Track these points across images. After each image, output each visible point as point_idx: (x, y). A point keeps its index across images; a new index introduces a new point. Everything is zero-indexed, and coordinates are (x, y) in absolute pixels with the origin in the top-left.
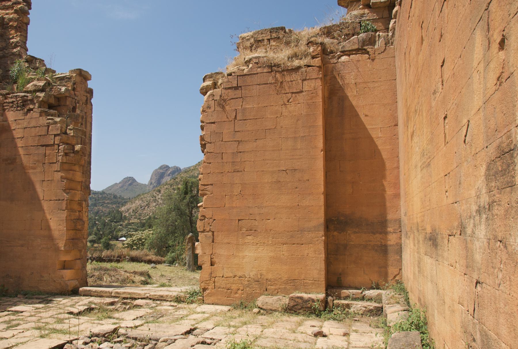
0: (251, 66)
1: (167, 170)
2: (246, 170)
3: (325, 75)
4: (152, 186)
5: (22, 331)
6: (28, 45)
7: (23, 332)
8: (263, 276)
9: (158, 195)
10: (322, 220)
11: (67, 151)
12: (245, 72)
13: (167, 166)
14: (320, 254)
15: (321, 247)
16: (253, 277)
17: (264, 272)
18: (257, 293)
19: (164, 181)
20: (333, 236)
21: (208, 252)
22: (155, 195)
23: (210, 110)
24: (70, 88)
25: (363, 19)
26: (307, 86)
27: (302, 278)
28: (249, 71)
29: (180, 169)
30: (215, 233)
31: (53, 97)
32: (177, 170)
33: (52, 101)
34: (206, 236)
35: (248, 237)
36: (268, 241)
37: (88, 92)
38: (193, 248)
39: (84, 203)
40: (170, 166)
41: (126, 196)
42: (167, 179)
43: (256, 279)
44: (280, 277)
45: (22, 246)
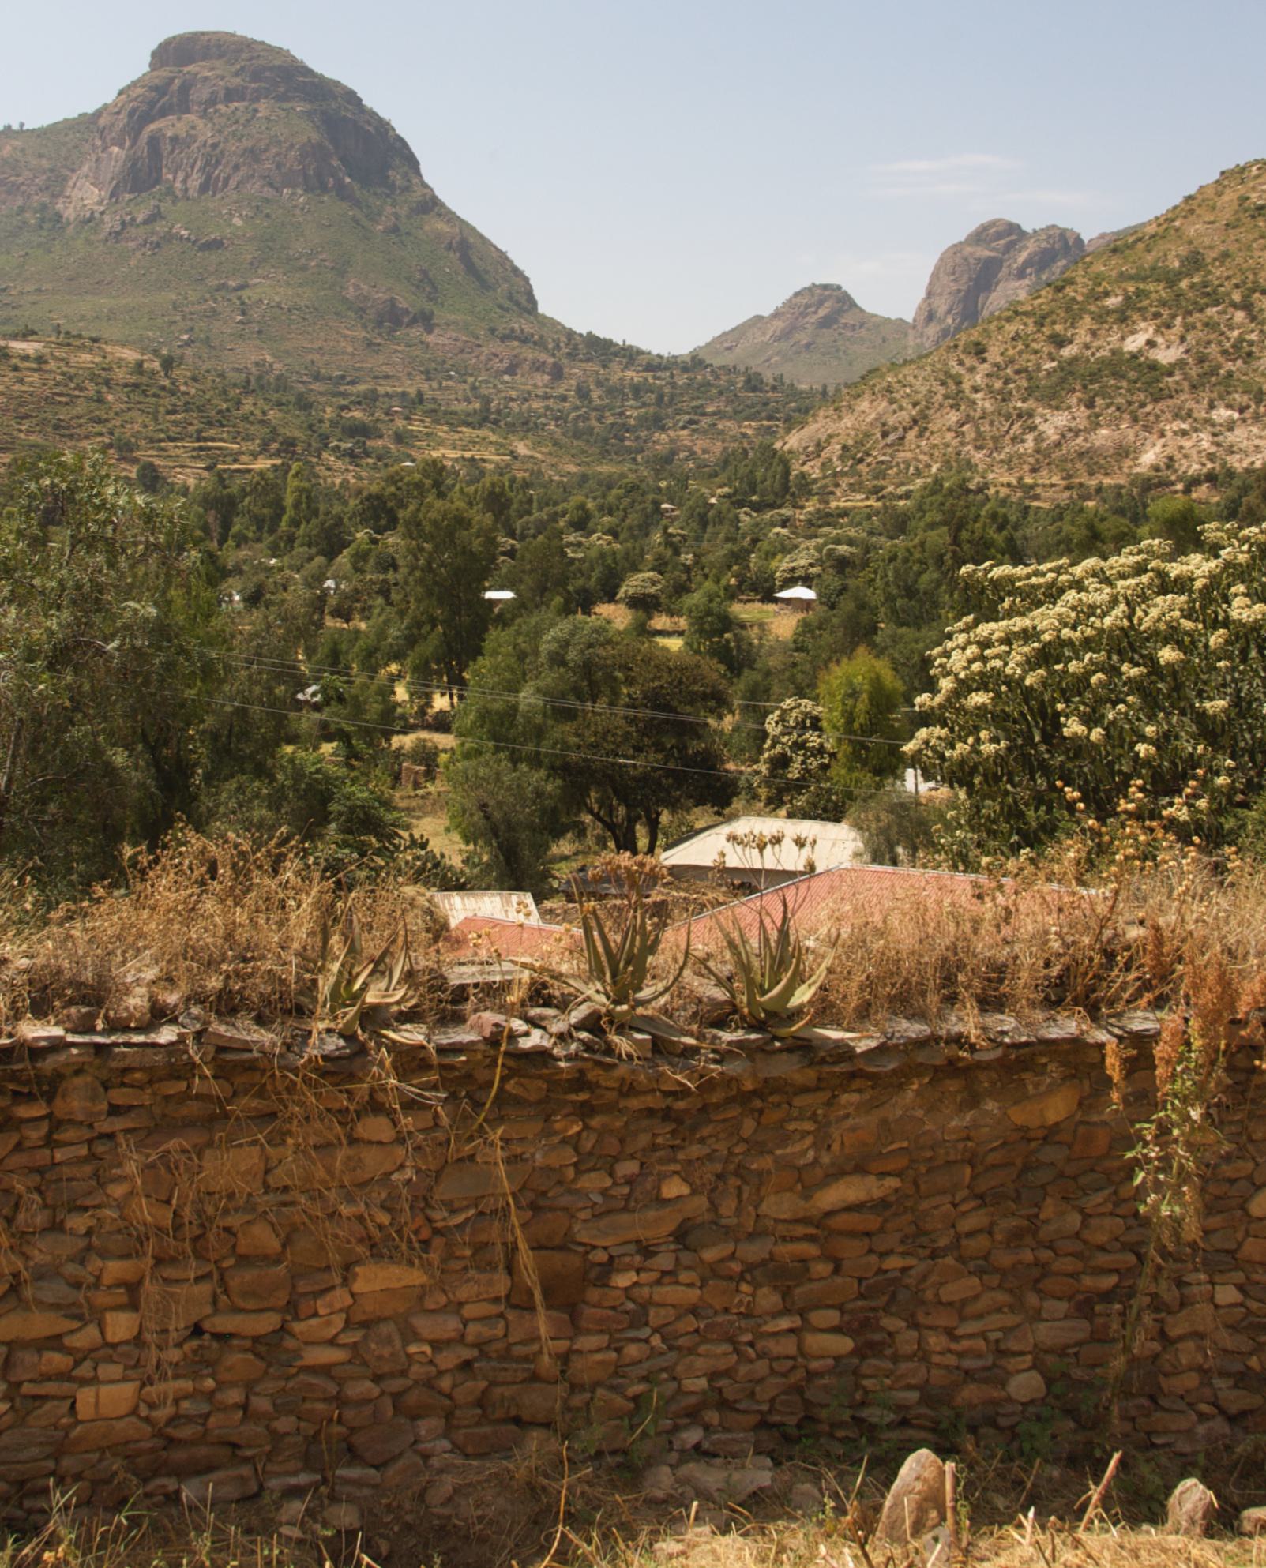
1: (1010, 246)
9: (972, 370)
29: (1078, 240)
32: (1062, 246)
40: (1028, 228)
41: (806, 377)
42: (1011, 291)
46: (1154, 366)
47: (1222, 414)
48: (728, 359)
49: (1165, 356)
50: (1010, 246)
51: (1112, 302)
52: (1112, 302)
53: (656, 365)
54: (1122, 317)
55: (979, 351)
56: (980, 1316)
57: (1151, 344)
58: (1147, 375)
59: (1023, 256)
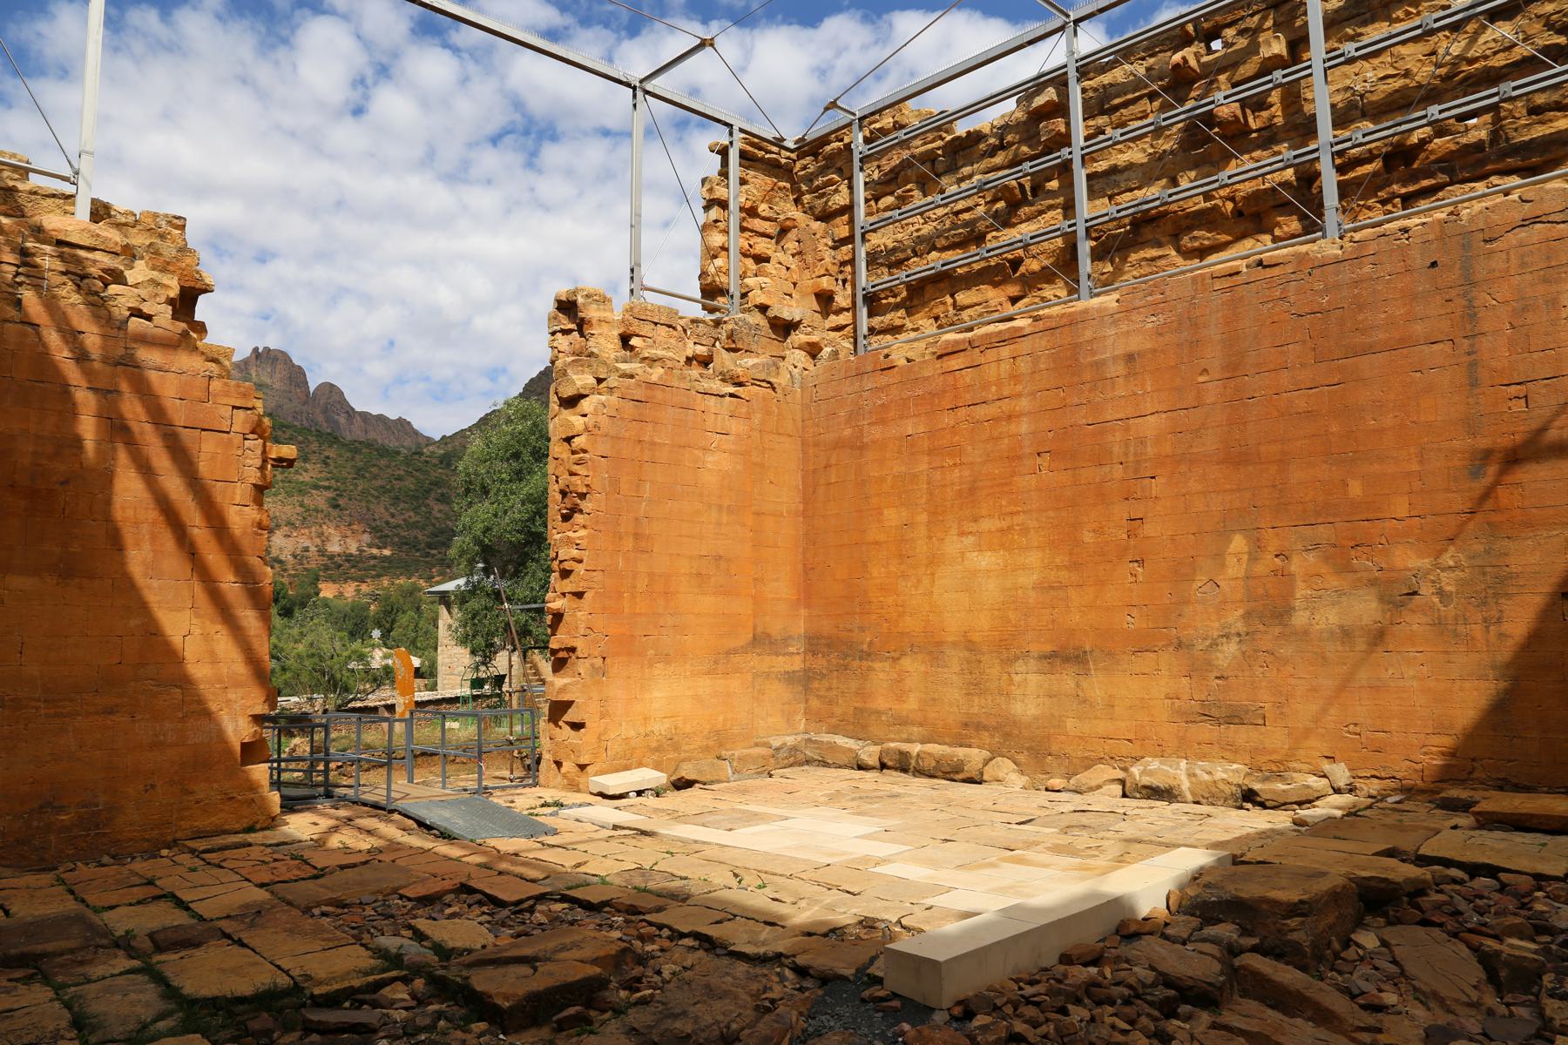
45: (110, 711)
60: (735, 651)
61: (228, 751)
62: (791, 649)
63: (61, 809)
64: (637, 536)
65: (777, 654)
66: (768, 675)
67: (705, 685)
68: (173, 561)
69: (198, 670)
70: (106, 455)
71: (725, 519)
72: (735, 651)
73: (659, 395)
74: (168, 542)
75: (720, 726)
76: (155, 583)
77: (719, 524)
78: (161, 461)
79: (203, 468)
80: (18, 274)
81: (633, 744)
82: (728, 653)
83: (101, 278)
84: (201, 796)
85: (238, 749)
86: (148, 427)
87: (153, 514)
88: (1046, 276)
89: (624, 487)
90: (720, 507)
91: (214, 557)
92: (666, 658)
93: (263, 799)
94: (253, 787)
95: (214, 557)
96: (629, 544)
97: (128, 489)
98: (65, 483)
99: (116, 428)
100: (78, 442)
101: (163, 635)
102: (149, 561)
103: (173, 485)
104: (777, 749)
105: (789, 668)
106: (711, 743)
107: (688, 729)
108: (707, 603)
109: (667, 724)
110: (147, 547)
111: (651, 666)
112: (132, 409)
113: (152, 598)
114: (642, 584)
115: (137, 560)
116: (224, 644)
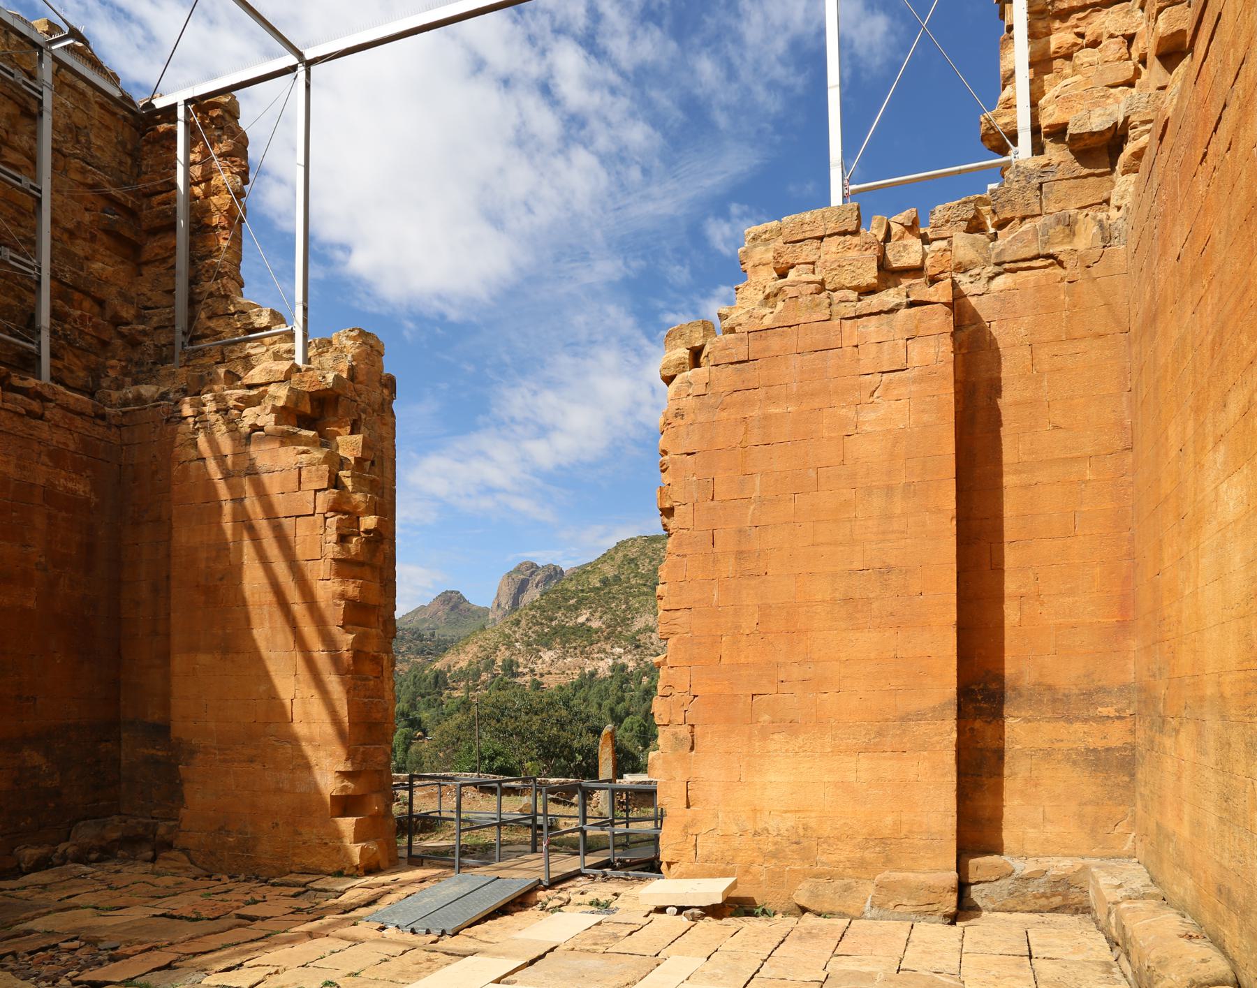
0: (780, 305)
1: (532, 573)
2: (770, 572)
3: (958, 326)
4: (500, 613)
5: (273, 970)
6: (243, 273)
7: (277, 972)
8: (809, 833)
9: (514, 632)
10: (951, 691)
11: (345, 531)
12: (767, 322)
13: (533, 565)
14: (944, 775)
15: (950, 758)
16: (786, 834)
17: (813, 823)
18: (794, 871)
19: (526, 599)
20: (972, 729)
21: (680, 776)
22: (507, 631)
23: (682, 422)
24: (345, 375)
25: (1050, 177)
26: (917, 352)
27: (902, 835)
28: (775, 320)
29: (562, 571)
30: (697, 730)
31: (307, 397)
32: (555, 573)
33: (307, 408)
34: (674, 734)
35: (776, 736)
36: (823, 747)
37: (385, 386)
38: (1182, 911)
39: (385, 656)
40: (539, 564)
41: (445, 632)
42: (533, 594)
43: (794, 838)
44: (850, 832)
45: (251, 760)
46: (589, 629)
47: (618, 650)
48: (413, 625)
49: (595, 624)
50: (532, 573)
51: (572, 602)
52: (572, 602)
53: (1101, 133)
54: (576, 608)
55: (517, 623)
56: (238, 500)
57: (588, 620)
58: (584, 632)
59: (538, 578)
60: (920, 716)
61: (322, 801)
62: (1103, 711)
63: (229, 833)
64: (740, 555)
65: (1069, 720)
66: (1048, 754)
67: (859, 769)
68: (284, 637)
69: (300, 728)
70: (239, 543)
71: (898, 507)
72: (920, 716)
73: (775, 343)
74: (279, 620)
75: (886, 832)
76: (272, 655)
77: (888, 517)
78: (272, 550)
79: (300, 551)
80: (195, 423)
81: (736, 842)
82: (905, 718)
83: (236, 407)
84: (306, 838)
85: (329, 800)
86: (264, 522)
87: (269, 597)
88: (46, 979)
89: (721, 491)
90: (889, 489)
91: (309, 630)
92: (790, 726)
93: (346, 849)
94: (339, 836)
95: (309, 630)
96: (728, 567)
97: (253, 580)
98: (221, 579)
99: (244, 522)
100: (174, 186)
101: (279, 699)
102: (267, 634)
103: (281, 568)
104: (1027, 879)
105: (1092, 742)
106: (869, 855)
107: (826, 831)
108: (866, 642)
109: (790, 821)
110: (267, 625)
111: (764, 738)
112: (252, 504)
113: (272, 668)
114: (748, 623)
115: (261, 634)
116: (317, 708)
